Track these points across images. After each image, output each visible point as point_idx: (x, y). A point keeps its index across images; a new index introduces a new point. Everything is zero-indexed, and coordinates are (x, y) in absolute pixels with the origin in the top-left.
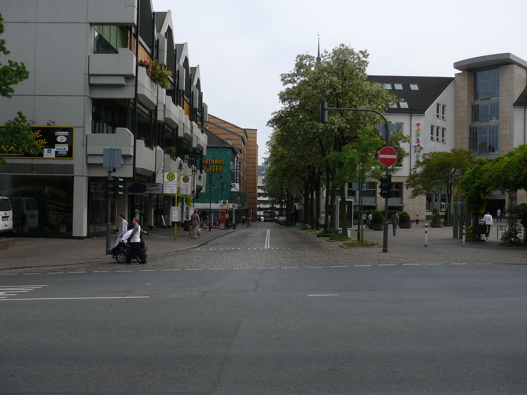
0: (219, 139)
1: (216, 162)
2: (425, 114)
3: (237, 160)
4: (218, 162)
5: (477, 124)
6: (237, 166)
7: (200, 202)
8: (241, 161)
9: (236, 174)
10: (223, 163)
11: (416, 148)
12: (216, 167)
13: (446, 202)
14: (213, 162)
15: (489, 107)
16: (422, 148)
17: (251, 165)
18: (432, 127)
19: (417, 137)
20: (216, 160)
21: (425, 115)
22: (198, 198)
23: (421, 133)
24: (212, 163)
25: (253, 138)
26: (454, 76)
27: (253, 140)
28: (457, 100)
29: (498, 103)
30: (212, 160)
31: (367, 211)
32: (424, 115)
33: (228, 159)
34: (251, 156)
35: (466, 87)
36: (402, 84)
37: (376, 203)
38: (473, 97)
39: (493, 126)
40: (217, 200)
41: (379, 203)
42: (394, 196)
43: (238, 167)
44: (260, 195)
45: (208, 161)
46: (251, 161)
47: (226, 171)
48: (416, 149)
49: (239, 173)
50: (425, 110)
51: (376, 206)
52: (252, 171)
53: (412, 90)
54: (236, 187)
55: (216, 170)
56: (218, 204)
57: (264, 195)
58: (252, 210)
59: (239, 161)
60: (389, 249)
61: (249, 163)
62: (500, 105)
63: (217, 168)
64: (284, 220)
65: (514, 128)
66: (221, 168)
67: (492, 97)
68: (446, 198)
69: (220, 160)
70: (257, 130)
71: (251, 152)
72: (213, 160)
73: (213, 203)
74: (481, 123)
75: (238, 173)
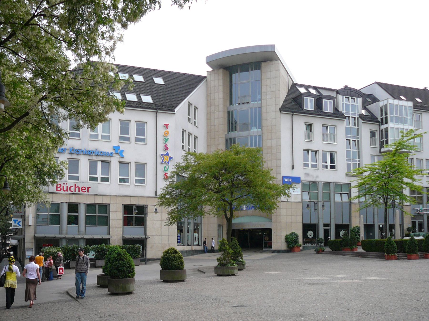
2: (175, 112)
5: (233, 134)
11: (163, 158)
13: (198, 233)
16: (171, 158)
18: (183, 132)
19: (165, 142)
21: (175, 114)
23: (169, 137)
26: (205, 74)
28: (209, 104)
29: (261, 108)
31: (96, 246)
32: (174, 113)
35: (221, 88)
36: (143, 76)
37: (109, 234)
38: (229, 101)
39: (254, 136)
41: (113, 234)
42: (134, 224)
48: (163, 159)
50: (175, 107)
51: (109, 239)
53: (157, 84)
62: (264, 110)
65: (281, 138)
67: (253, 101)
68: (199, 227)
74: (240, 133)
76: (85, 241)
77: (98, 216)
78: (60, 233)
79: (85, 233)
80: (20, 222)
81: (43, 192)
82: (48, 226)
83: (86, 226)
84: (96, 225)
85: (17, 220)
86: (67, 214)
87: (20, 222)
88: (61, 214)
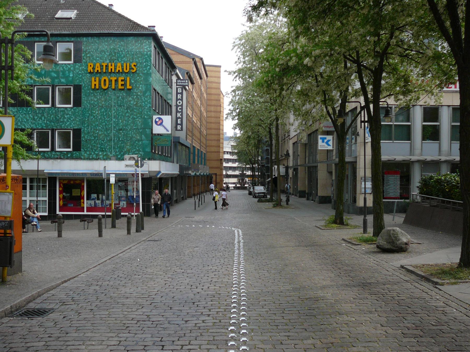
0: (128, 22)
1: (119, 68)
3: (177, 82)
4: (123, 69)
7: (84, 159)
8: (185, 83)
9: (177, 109)
14: (113, 67)
20: (119, 65)
24: (110, 71)
25: (215, 77)
27: (216, 80)
30: (110, 64)
33: (145, 62)
34: (214, 103)
43: (179, 95)
44: (228, 161)
46: (212, 109)
47: (142, 88)
52: (213, 123)
54: (163, 124)
55: (120, 87)
56: (123, 162)
57: (233, 161)
59: (182, 83)
63: (120, 83)
64: (263, 191)
69: (128, 64)
70: (220, 67)
71: (213, 97)
72: (113, 64)
75: (180, 106)
76: (449, 168)
77: (395, 125)
78: (412, 152)
79: (449, 152)
80: (329, 141)
81: (12, 94)
82: (393, 142)
83: (452, 142)
84: (392, 140)
85: (326, 138)
86: (422, 123)
87: (329, 141)
88: (412, 125)
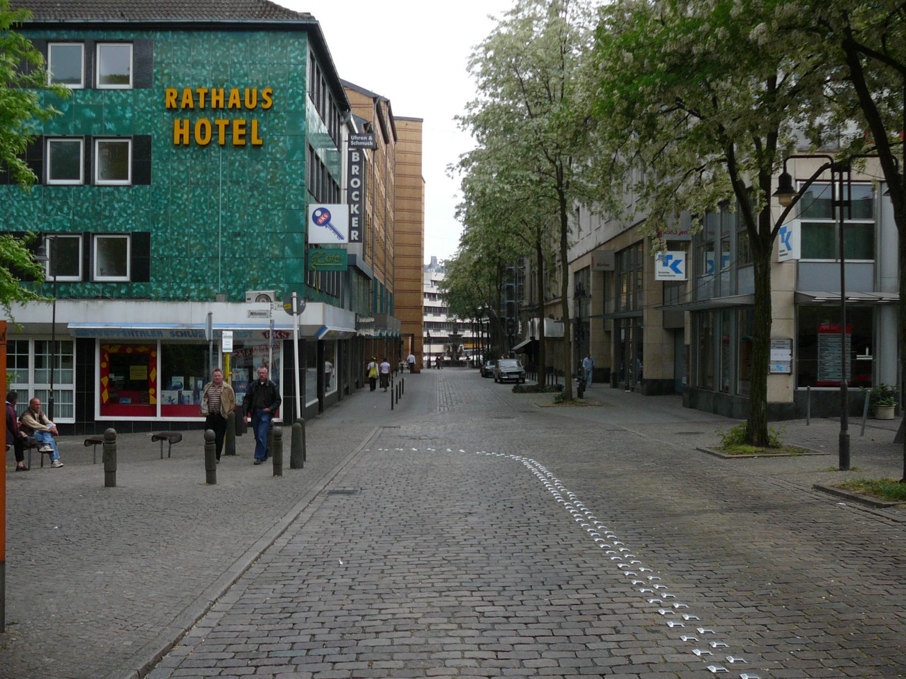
3: (349, 140)
4: (243, 102)
6: (351, 163)
7: (157, 299)
9: (349, 196)
10: (266, 102)
12: (236, 124)
15: (349, 376)
17: (406, 216)
20: (235, 92)
22: (148, 280)
25: (411, 141)
27: (412, 147)
30: (214, 92)
34: (408, 193)
40: (241, 286)
43: (353, 167)
45: (196, 95)
46: (406, 204)
49: (359, 189)
52: (408, 233)
54: (332, 222)
55: (237, 141)
56: (243, 304)
57: (437, 311)
58: (412, 342)
60: (853, 461)
61: (402, 210)
63: (237, 132)
66: (259, 128)
70: (421, 120)
72: (221, 91)
73: (220, 301)
